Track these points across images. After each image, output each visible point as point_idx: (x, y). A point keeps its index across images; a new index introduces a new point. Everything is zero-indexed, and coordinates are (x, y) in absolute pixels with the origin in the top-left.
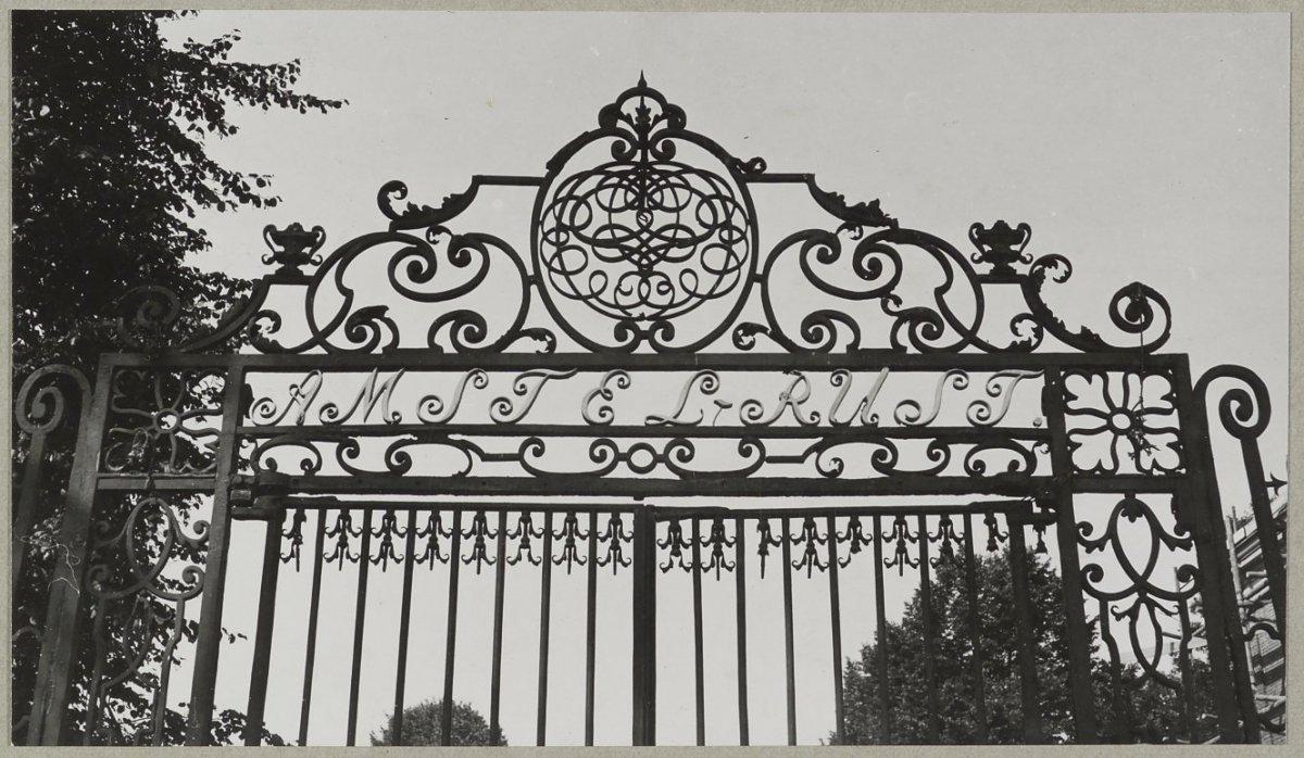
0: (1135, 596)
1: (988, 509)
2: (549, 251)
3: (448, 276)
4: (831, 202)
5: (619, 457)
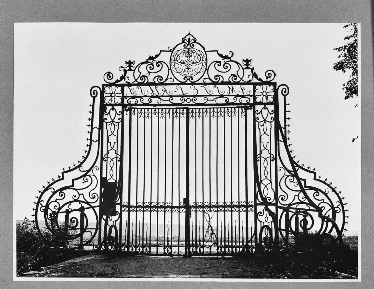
0: (264, 122)
1: (238, 107)
2: (173, 64)
3: (156, 69)
4: (221, 55)
5: (185, 100)
